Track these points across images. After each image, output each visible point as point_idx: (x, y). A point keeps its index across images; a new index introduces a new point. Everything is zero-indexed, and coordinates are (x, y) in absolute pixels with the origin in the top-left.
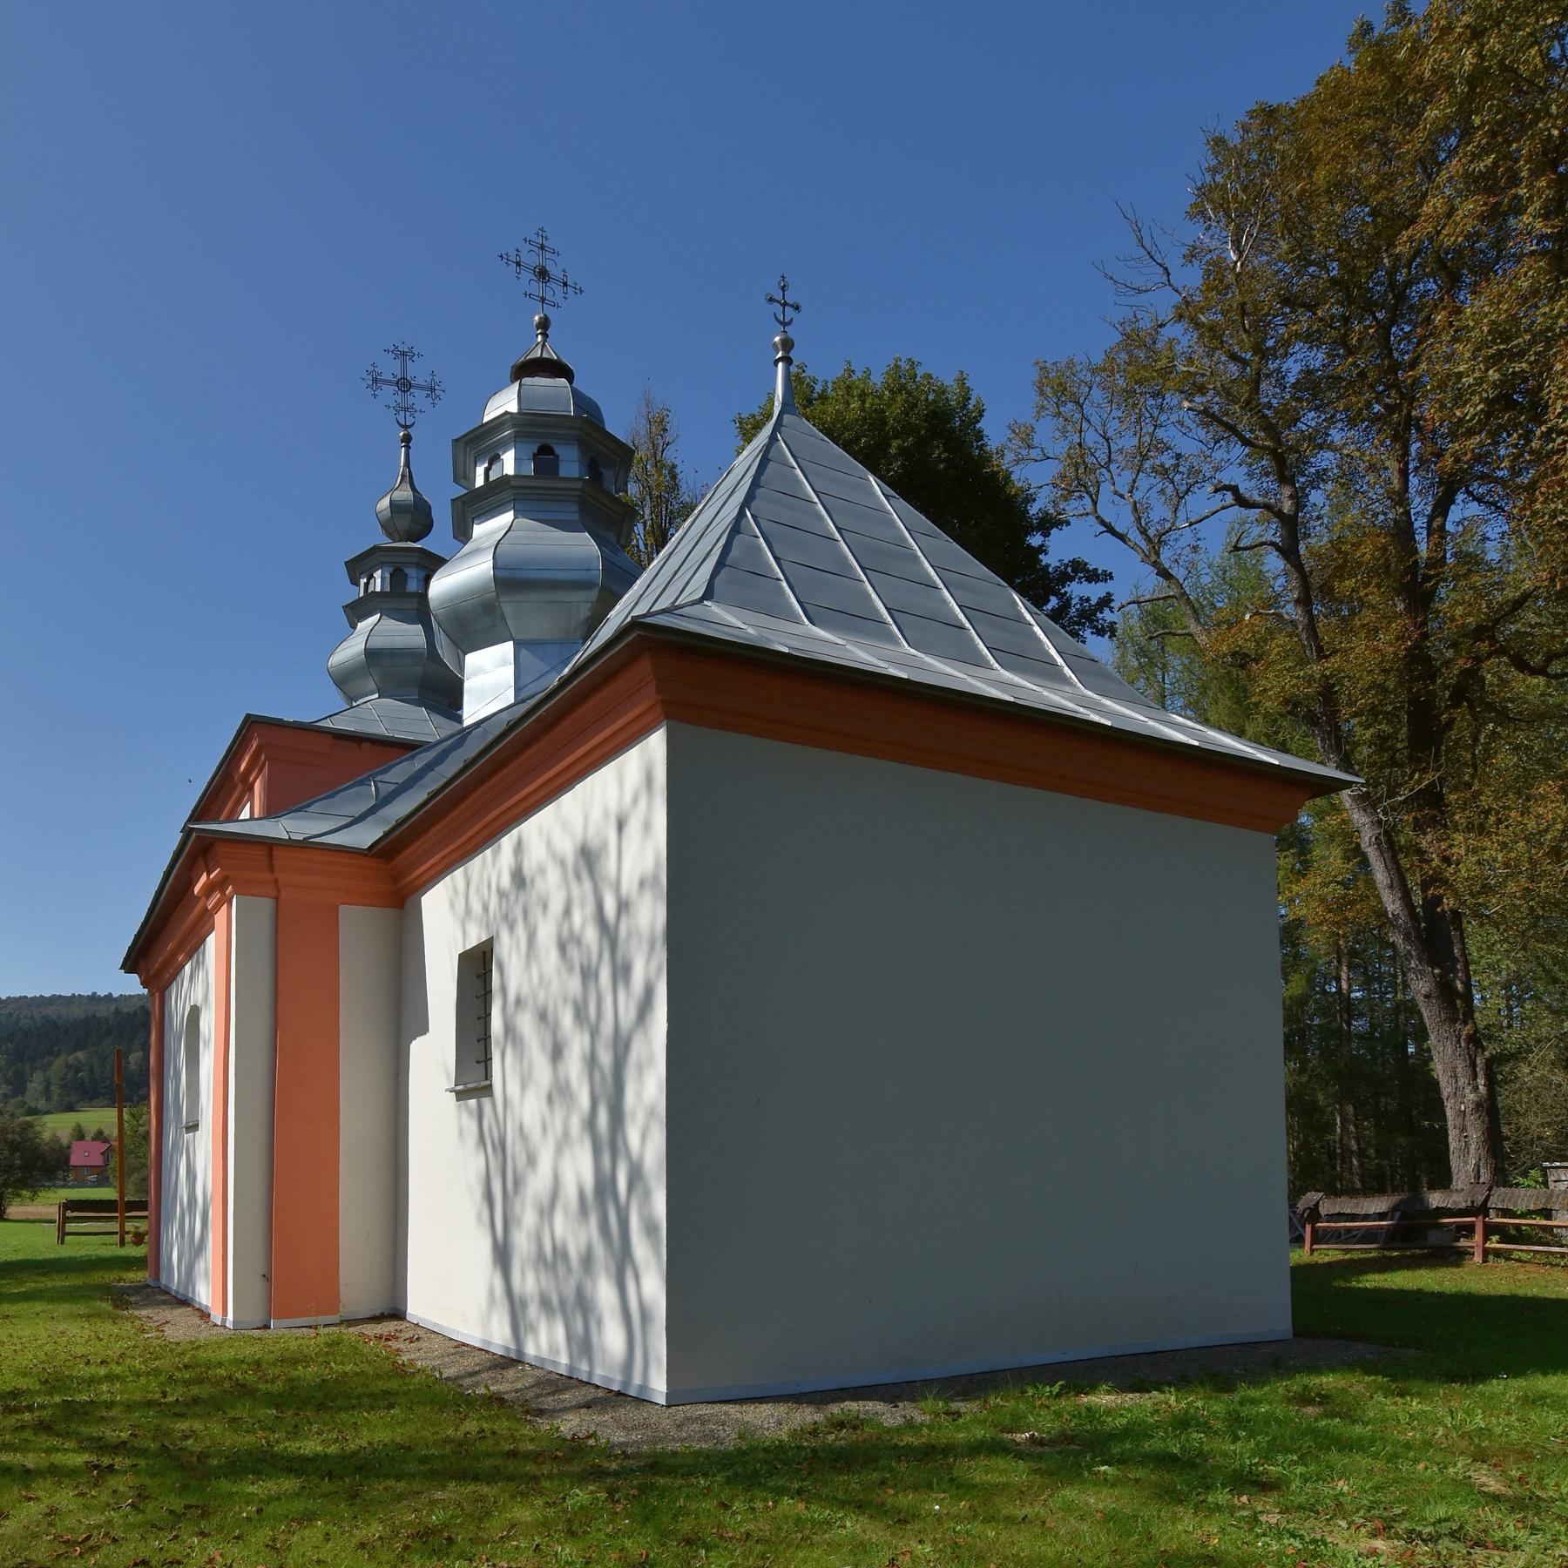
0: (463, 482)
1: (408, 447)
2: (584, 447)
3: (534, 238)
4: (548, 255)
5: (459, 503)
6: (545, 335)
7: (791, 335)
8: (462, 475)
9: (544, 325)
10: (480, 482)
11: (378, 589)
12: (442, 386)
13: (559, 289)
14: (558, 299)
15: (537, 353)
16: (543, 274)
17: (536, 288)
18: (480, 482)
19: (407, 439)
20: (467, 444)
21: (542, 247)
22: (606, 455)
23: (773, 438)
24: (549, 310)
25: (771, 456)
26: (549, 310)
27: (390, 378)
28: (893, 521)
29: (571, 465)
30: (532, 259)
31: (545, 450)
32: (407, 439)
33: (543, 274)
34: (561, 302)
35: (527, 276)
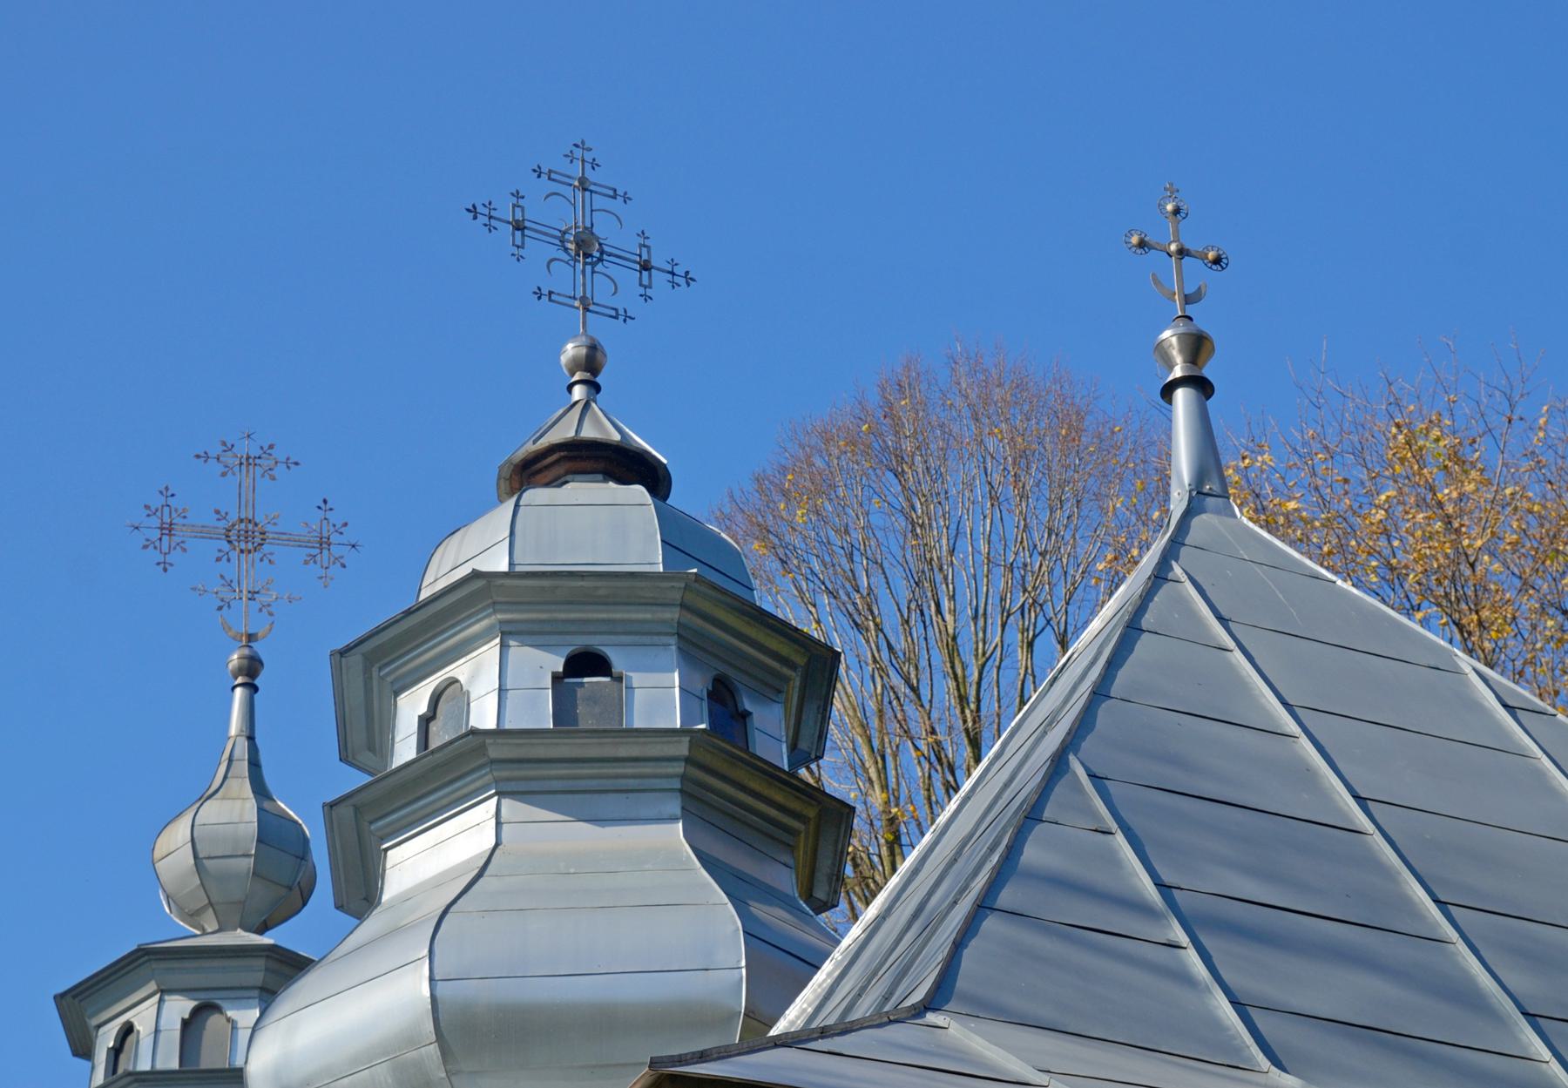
0: (366, 757)
1: (252, 688)
2: (692, 647)
3: (563, 166)
4: (599, 202)
5: (346, 811)
6: (594, 387)
7: (1202, 324)
8: (362, 732)
9: (591, 364)
10: (405, 750)
11: (144, 1065)
12: (350, 535)
13: (629, 278)
14: (628, 298)
15: (565, 432)
16: (586, 248)
17: (565, 278)
18: (405, 750)
19: (251, 669)
20: (370, 660)
21: (584, 185)
22: (759, 670)
23: (1160, 575)
24: (603, 330)
25: (1147, 621)
26: (603, 330)
27: (210, 520)
28: (1541, 775)
29: (659, 696)
30: (561, 214)
31: (586, 663)
32: (251, 669)
33: (586, 248)
34: (635, 307)
35: (538, 251)
